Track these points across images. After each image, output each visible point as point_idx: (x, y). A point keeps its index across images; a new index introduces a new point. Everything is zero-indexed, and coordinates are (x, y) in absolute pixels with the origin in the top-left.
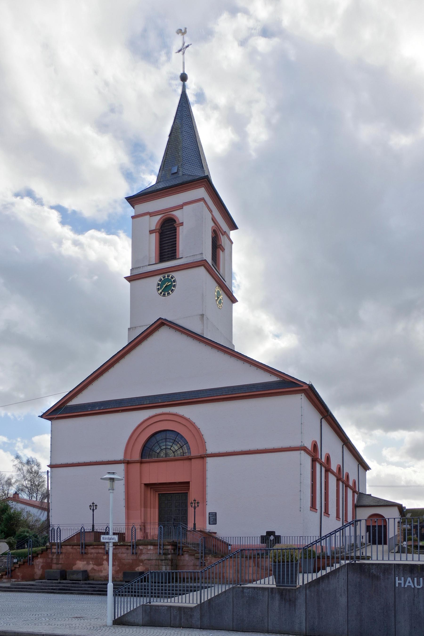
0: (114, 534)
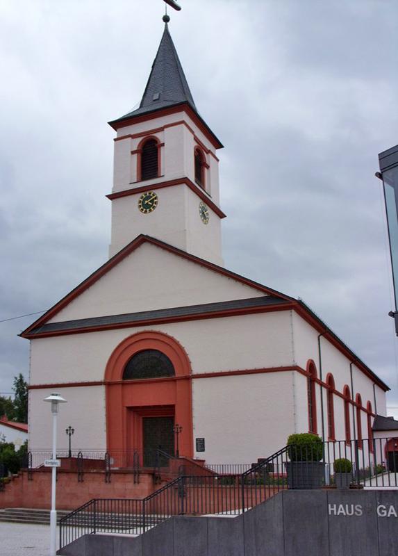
0: (57, 458)
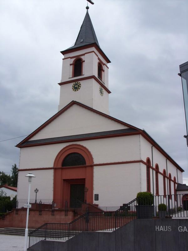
0: (30, 204)
